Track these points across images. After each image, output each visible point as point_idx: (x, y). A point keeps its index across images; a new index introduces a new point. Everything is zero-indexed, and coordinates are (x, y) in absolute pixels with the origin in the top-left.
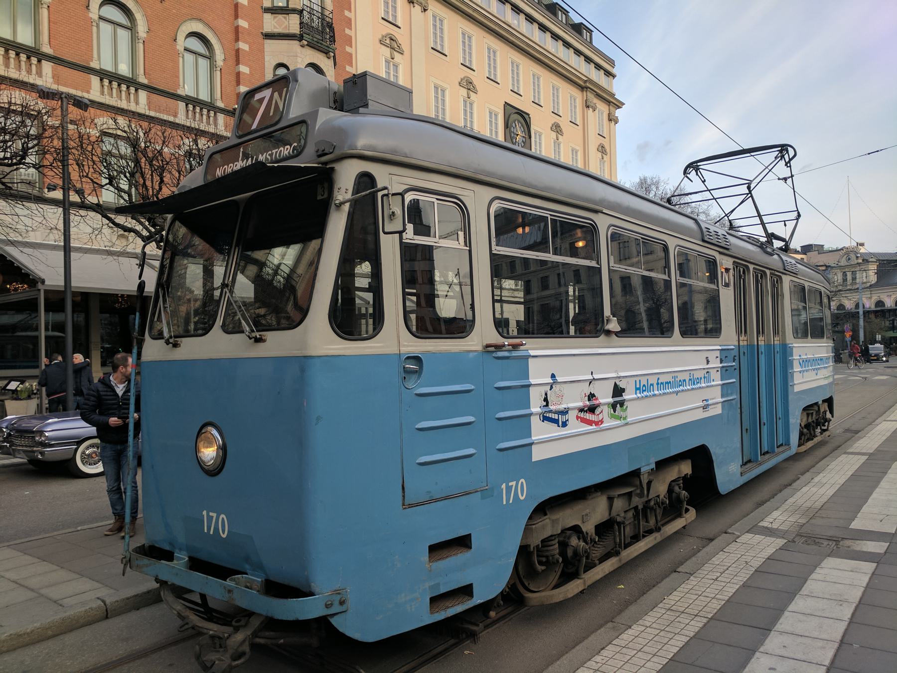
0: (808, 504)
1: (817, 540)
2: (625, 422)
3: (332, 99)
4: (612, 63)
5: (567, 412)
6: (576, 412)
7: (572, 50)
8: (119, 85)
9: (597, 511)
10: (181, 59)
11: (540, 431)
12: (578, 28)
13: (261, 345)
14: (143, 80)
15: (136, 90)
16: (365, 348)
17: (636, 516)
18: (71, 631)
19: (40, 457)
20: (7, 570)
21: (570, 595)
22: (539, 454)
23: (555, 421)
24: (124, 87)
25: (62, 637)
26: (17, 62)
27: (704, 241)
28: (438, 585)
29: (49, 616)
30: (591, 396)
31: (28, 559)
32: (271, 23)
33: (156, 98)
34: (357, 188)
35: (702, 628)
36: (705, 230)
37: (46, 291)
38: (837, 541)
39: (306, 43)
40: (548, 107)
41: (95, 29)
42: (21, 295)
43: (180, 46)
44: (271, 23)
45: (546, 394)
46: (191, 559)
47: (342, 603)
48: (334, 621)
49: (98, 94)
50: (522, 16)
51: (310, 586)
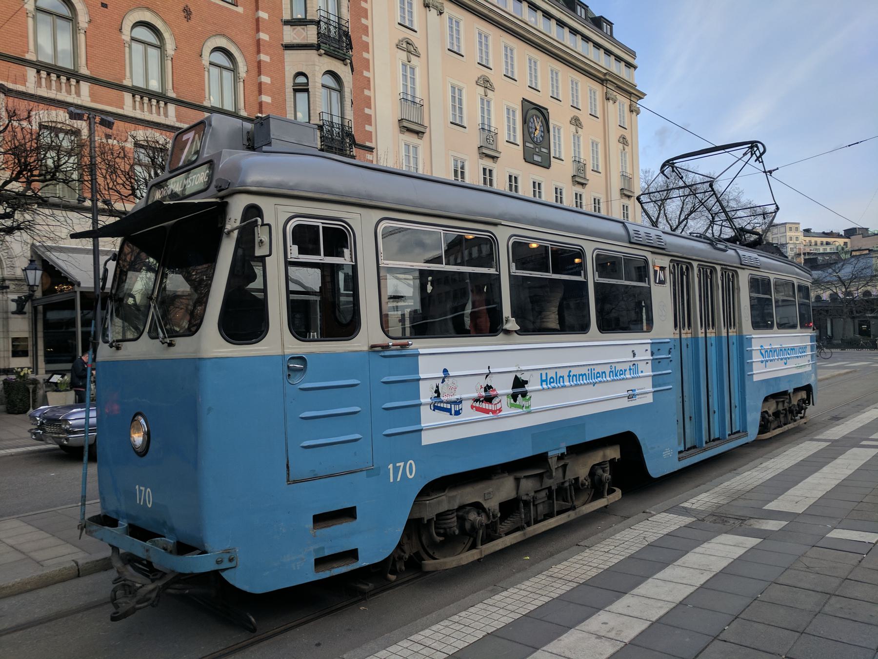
0: (739, 488)
1: (725, 519)
2: (528, 410)
4: (633, 54)
5: (461, 402)
9: (504, 490)
10: (206, 73)
11: (429, 418)
12: (598, 22)
14: (171, 94)
16: (251, 350)
17: (550, 497)
18: (47, 586)
20: (9, 537)
21: (464, 562)
22: (428, 439)
24: (154, 102)
25: (38, 591)
27: (631, 243)
28: (323, 548)
29: (31, 573)
30: (488, 388)
32: (290, 35)
33: (183, 110)
35: (568, 591)
37: (81, 293)
39: (323, 52)
40: (567, 100)
41: (127, 49)
42: (65, 296)
43: (205, 61)
44: (290, 35)
45: (437, 387)
46: (130, 525)
47: (231, 560)
48: (225, 575)
49: (131, 109)
50: (540, 13)
51: (204, 546)
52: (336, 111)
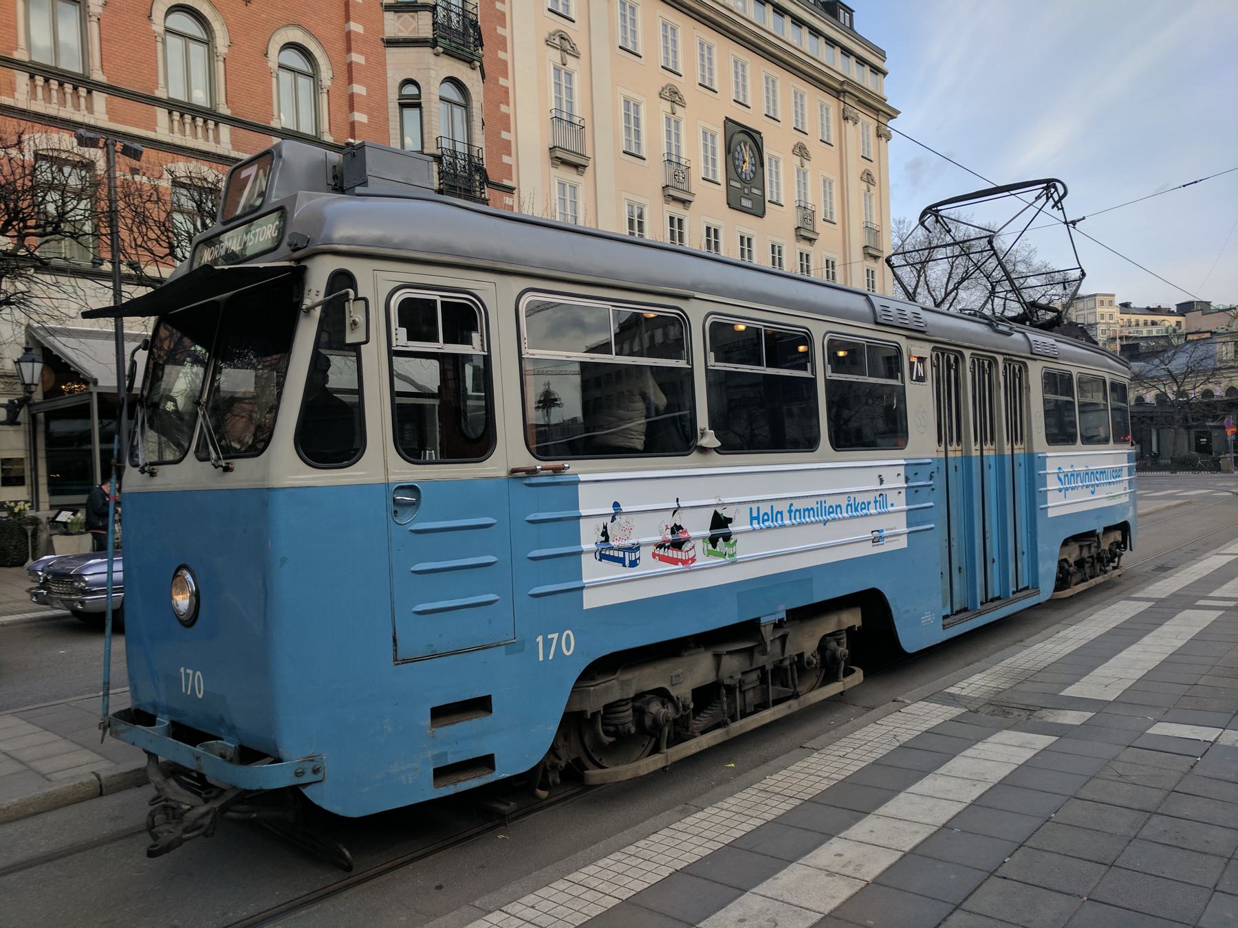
1: (1007, 710)
3: (330, 175)
4: (881, 54)
5: (638, 549)
6: (652, 548)
7: (822, 40)
8: (193, 119)
9: (699, 670)
10: (274, 80)
11: (593, 570)
13: (229, 475)
14: (224, 110)
15: (216, 124)
17: (763, 680)
19: (79, 607)
22: (591, 600)
23: (621, 561)
24: (200, 121)
25: (44, 815)
26: (61, 95)
27: (877, 323)
28: (445, 754)
29: (33, 790)
30: (676, 529)
31: (30, 728)
32: (395, 25)
33: (242, 133)
34: (330, 288)
36: (878, 309)
37: (99, 394)
38: (1030, 710)
39: (441, 50)
41: (160, 46)
42: (78, 399)
44: (395, 25)
45: (605, 527)
46: (174, 724)
48: (307, 792)
49: (167, 132)
52: (460, 135)
